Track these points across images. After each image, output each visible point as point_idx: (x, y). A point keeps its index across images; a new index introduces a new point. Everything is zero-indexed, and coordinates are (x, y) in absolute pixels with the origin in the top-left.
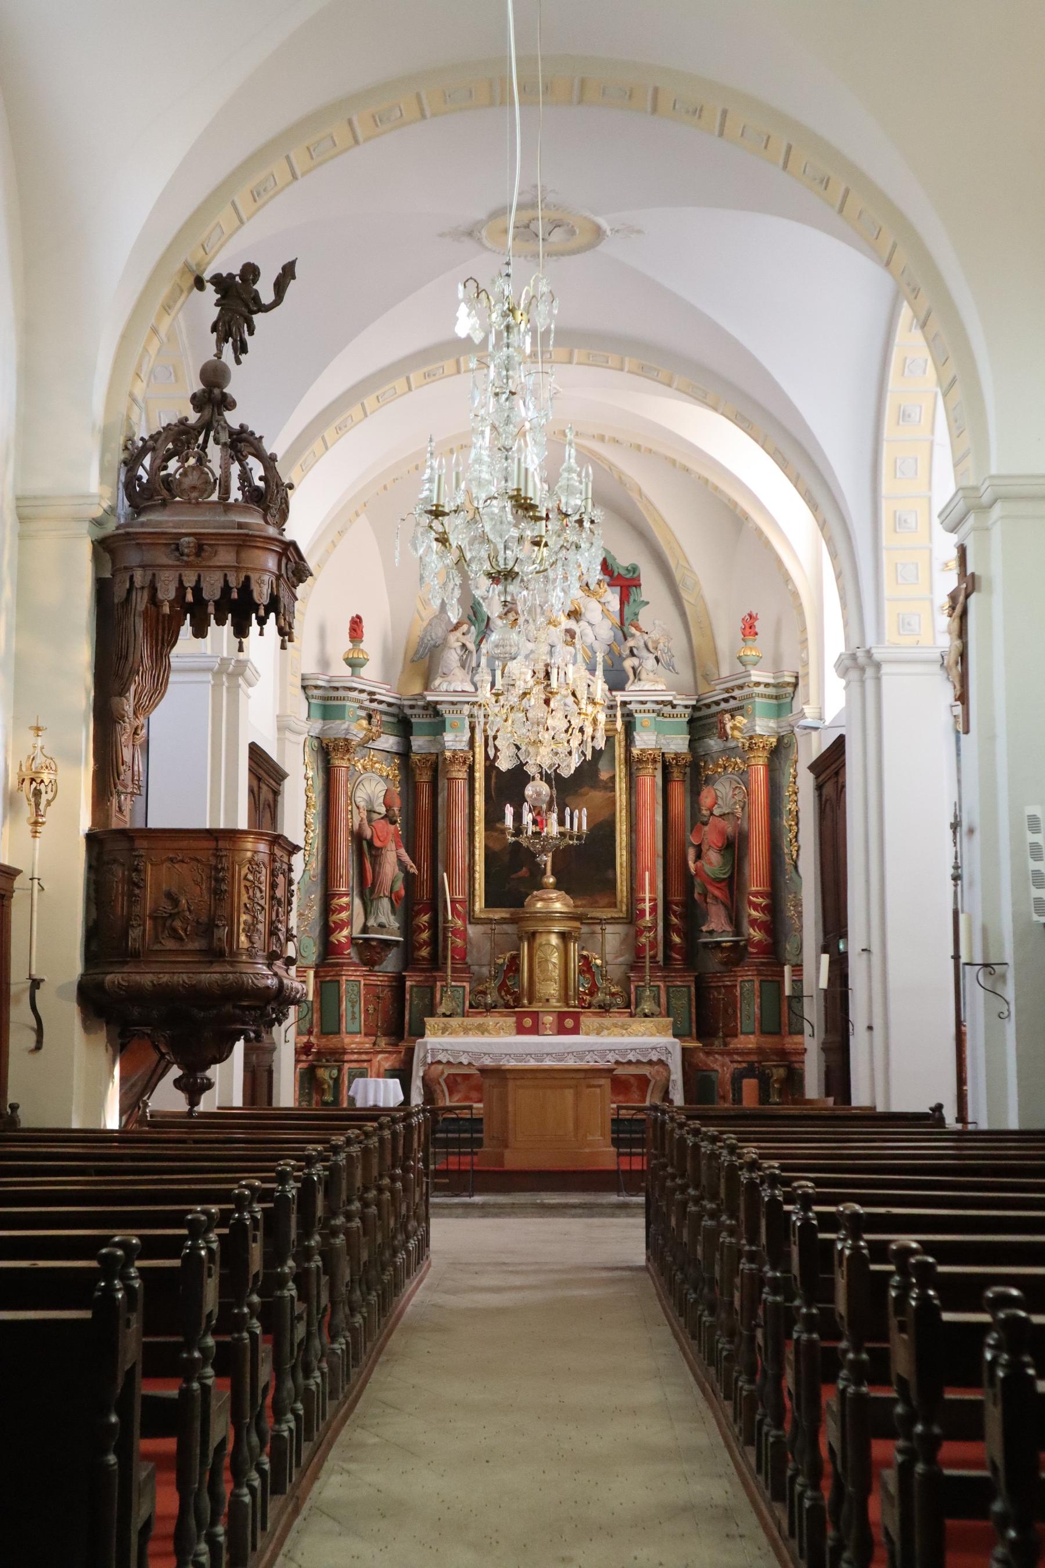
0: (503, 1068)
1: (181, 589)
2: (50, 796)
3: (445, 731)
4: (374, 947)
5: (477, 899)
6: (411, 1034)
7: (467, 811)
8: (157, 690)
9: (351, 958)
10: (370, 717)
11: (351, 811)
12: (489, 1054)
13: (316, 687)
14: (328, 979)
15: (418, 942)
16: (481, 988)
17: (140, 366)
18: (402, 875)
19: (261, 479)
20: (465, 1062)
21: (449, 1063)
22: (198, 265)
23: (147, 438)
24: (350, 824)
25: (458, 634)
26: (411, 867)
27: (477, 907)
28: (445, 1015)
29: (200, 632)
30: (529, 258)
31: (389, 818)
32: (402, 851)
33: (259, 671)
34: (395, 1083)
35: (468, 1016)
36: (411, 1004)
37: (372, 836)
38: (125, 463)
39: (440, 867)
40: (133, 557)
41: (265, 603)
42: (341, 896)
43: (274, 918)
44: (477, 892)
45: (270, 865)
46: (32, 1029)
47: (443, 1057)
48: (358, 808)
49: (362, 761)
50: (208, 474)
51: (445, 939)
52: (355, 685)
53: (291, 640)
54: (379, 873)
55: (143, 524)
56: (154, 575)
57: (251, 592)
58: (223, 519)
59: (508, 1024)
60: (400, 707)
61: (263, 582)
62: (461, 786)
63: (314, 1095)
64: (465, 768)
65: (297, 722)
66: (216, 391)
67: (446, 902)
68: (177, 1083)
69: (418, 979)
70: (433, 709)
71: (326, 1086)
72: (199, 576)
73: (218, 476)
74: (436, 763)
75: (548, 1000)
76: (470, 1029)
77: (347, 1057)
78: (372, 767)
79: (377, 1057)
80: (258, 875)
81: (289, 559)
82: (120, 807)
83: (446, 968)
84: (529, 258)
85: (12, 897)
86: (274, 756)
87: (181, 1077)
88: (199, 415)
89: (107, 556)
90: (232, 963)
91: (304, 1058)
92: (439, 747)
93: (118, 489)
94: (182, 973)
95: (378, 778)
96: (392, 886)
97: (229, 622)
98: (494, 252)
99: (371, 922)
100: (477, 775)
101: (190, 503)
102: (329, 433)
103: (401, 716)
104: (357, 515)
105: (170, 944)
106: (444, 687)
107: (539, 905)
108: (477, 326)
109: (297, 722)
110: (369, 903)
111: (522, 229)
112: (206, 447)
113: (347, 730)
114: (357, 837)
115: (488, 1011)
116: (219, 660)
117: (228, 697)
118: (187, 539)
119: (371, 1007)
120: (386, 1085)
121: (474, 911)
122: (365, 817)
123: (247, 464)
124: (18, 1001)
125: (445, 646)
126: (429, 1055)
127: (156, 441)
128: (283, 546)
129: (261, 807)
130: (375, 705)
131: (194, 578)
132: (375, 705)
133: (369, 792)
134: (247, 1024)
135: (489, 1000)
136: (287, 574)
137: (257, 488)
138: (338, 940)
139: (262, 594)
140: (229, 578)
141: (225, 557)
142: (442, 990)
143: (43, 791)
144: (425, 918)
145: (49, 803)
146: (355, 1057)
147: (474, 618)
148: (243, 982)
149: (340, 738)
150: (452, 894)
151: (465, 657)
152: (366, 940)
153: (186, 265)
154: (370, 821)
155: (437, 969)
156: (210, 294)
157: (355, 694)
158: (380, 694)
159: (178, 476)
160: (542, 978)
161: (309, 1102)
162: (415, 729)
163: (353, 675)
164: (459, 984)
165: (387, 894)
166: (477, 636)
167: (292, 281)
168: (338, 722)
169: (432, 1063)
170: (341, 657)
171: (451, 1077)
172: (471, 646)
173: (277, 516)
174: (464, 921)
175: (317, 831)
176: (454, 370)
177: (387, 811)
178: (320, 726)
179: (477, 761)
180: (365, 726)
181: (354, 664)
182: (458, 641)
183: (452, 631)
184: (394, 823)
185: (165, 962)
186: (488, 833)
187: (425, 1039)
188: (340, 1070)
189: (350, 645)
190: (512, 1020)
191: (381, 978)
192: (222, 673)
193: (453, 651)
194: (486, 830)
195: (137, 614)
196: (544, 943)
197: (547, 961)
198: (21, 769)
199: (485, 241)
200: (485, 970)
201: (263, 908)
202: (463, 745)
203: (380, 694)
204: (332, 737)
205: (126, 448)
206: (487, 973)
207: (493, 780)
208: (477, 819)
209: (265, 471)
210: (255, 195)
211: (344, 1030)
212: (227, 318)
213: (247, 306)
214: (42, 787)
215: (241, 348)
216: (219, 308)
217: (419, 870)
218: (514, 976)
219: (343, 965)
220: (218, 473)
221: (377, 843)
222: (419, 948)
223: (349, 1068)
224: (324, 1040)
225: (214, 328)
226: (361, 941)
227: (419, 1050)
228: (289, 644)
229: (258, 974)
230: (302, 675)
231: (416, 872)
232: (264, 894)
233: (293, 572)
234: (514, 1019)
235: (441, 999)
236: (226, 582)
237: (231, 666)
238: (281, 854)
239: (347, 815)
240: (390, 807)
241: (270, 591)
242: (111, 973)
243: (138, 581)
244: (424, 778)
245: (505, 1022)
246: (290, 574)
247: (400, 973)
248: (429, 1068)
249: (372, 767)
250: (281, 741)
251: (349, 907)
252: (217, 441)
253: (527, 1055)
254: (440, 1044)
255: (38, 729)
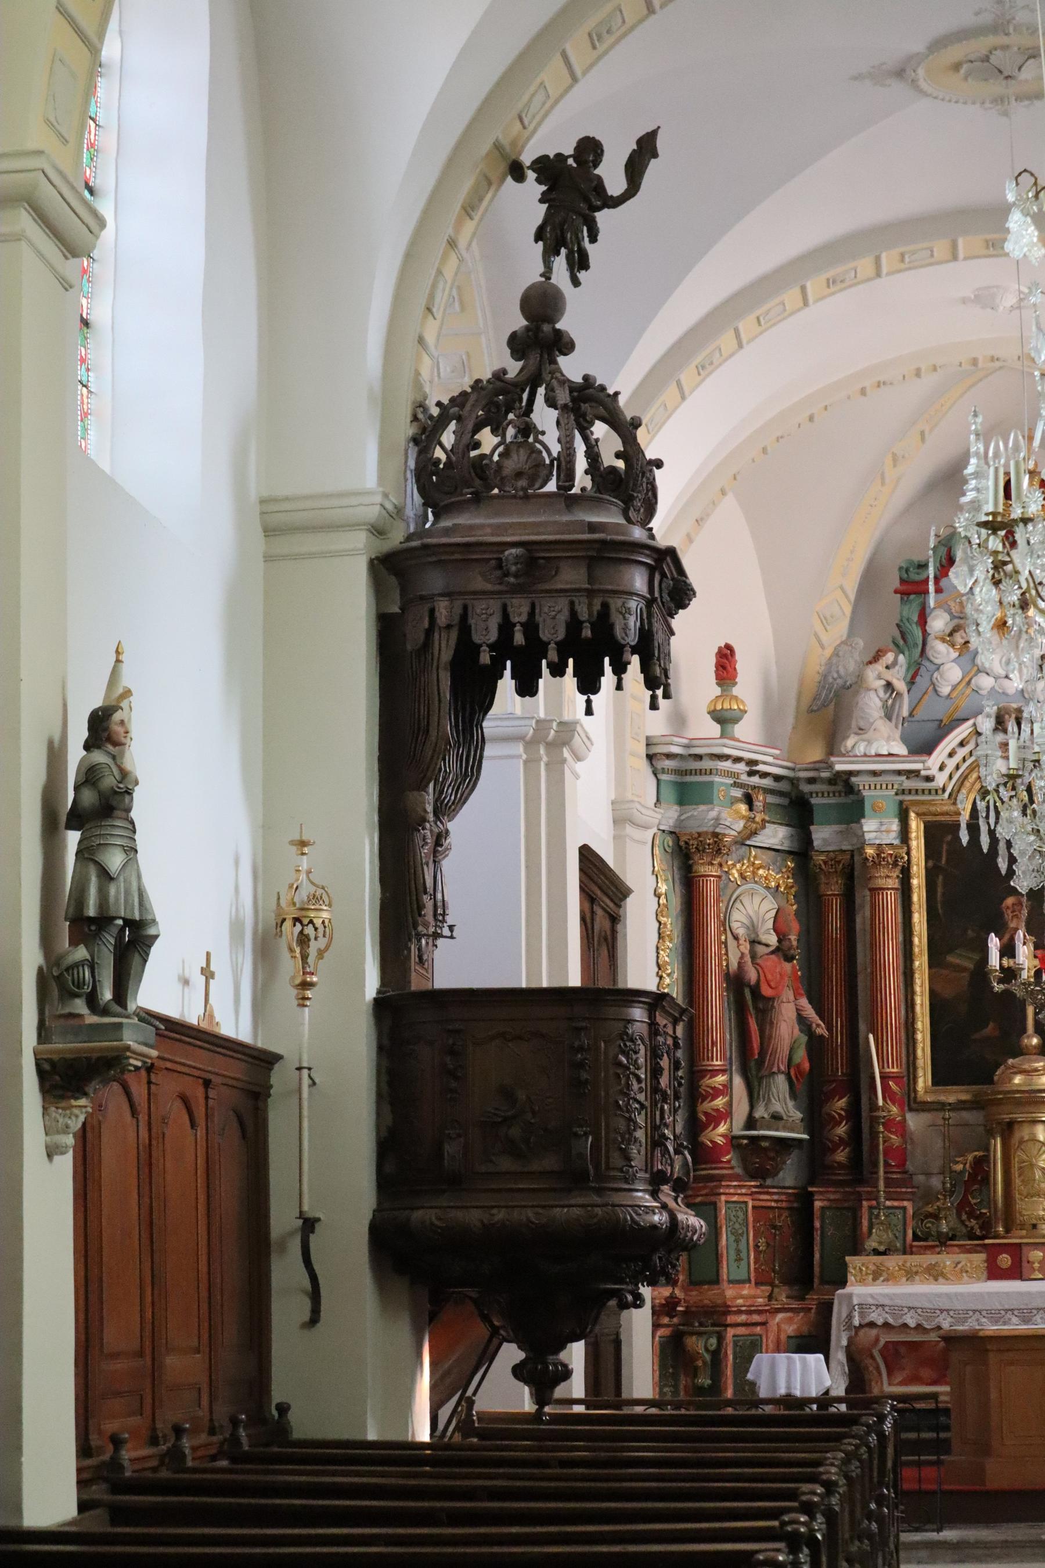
0: (981, 1334)
1: (506, 627)
2: (322, 943)
3: (863, 816)
4: (765, 1149)
5: (920, 1073)
6: (823, 1281)
7: (901, 938)
8: (466, 775)
9: (732, 1168)
10: (749, 800)
11: (726, 943)
12: (948, 1311)
13: (669, 756)
14: (698, 1200)
15: (832, 1141)
16: (930, 1209)
17: (431, 296)
18: (804, 1039)
19: (618, 455)
20: (912, 1323)
21: (886, 1325)
22: (514, 143)
23: (446, 401)
24: (724, 964)
25: (879, 667)
26: (818, 1025)
27: (920, 1084)
28: (876, 1252)
29: (527, 688)
30: (987, 105)
31: (782, 951)
32: (804, 1002)
33: (591, 736)
34: (817, 1360)
35: (912, 1253)
36: (822, 1233)
37: (758, 981)
38: (415, 440)
39: (862, 1027)
40: (434, 581)
41: (633, 644)
42: (715, 1073)
43: (658, 1122)
44: (920, 1062)
45: (650, 1040)
46: (305, 1292)
47: (877, 1317)
48: (736, 938)
49: (738, 866)
50: (541, 452)
51: (874, 1135)
52: (727, 751)
53: (667, 696)
54: (770, 1037)
55: (447, 532)
56: (465, 608)
57: (612, 626)
58: (566, 518)
59: (975, 1264)
60: (793, 781)
61: (629, 611)
62: (891, 900)
63: (682, 1377)
64: (896, 872)
65: (643, 811)
66: (546, 328)
67: (873, 1078)
68: (519, 1372)
69: (832, 1197)
70: (844, 783)
71: (700, 1363)
72: (533, 606)
73: (555, 454)
74: (851, 866)
75: (1034, 1226)
76: (916, 1273)
77: (731, 1319)
78: (754, 873)
79: (774, 1319)
80: (634, 1057)
81: (663, 575)
82: (420, 957)
83: (877, 1179)
84: (987, 105)
85: (269, 1095)
86: (610, 860)
87: (523, 1363)
88: (520, 364)
89: (393, 580)
90: (599, 1191)
91: (666, 1320)
92: (855, 840)
93: (406, 480)
94: (525, 1207)
95: (762, 891)
96: (790, 1060)
97: (570, 670)
98: (936, 98)
99: (760, 1112)
100: (915, 882)
101: (514, 497)
102: (687, 376)
103: (793, 795)
104: (723, 492)
105: (506, 1164)
106: (861, 749)
107: (1017, 1080)
108: (1035, 240)
109: (643, 811)
110: (756, 1083)
111: (978, 64)
112: (532, 411)
113: (717, 819)
114: (736, 982)
115: (943, 1244)
116: (534, 721)
117: (548, 776)
118: (513, 551)
119: (762, 1240)
120: (804, 1364)
121: (915, 1091)
122: (747, 952)
123: (592, 433)
124: (283, 1248)
125: (860, 687)
126: (856, 1314)
127: (462, 406)
128: (655, 556)
129: (596, 939)
130: (755, 780)
131: (525, 609)
132: (755, 780)
133: (751, 913)
134: (621, 1281)
135: (944, 1229)
136: (661, 597)
137: (613, 469)
138: (712, 1142)
139: (629, 627)
140: (578, 608)
141: (572, 576)
142: (871, 1214)
143: (312, 937)
144: (841, 1103)
145: (321, 954)
146: (743, 1318)
147: (901, 642)
148: (618, 1219)
149: (706, 833)
150: (882, 1067)
151: (890, 702)
152: (754, 1139)
153: (497, 146)
154: (753, 956)
155: (860, 1181)
156: (533, 188)
157: (727, 765)
158: (765, 763)
159: (496, 458)
160: (1025, 1193)
161: (676, 1387)
162: (817, 816)
163: (723, 735)
164: (896, 1204)
165: (782, 1068)
166: (908, 670)
167: (653, 161)
168: (702, 808)
169: (861, 1326)
170: (705, 711)
171: (891, 1346)
172: (900, 685)
173: (642, 510)
174: (902, 1109)
175: (675, 976)
176: (871, 271)
177: (779, 941)
178: (675, 815)
179: (914, 860)
180: (744, 813)
181: (724, 719)
182: (879, 678)
183: (870, 663)
184: (789, 959)
185: (499, 1191)
186: (933, 970)
187: (848, 1289)
188: (721, 1338)
189: (718, 691)
190: (980, 1258)
191: (775, 1197)
192: (539, 742)
193: (872, 694)
194: (930, 967)
195: (442, 665)
196: (1026, 1138)
197: (1032, 1166)
198: (278, 904)
199: (923, 84)
200: (936, 1182)
201: (642, 1106)
202: (891, 836)
203: (765, 763)
204: (694, 831)
205: (415, 418)
206: (940, 1186)
207: (940, 890)
208: (916, 950)
209: (624, 443)
210: (594, 39)
211: (725, 1277)
212: (558, 220)
213: (587, 200)
214: (309, 930)
215: (579, 262)
216: (546, 205)
217: (829, 1028)
218: (981, 1191)
219: (720, 1178)
220: (556, 449)
221: (766, 991)
222: (834, 1150)
223: (734, 1336)
224: (694, 1293)
225: (539, 236)
226: (745, 1141)
227: (840, 1304)
228: (661, 701)
229: (639, 1206)
230: (648, 738)
231: (826, 1034)
232: (643, 1085)
233: (669, 595)
234: (983, 1256)
235: (871, 1227)
236: (573, 613)
237: (552, 732)
238: (665, 1022)
239: (720, 948)
240: (784, 936)
241: (638, 624)
242: (423, 1207)
243: (442, 618)
244: (833, 888)
245: (971, 1262)
246: (666, 598)
247: (805, 1188)
248: (856, 1334)
249: (754, 873)
250: (619, 839)
251: (727, 1088)
252: (551, 402)
253: (1006, 1311)
254: (872, 1296)
255: (303, 844)
